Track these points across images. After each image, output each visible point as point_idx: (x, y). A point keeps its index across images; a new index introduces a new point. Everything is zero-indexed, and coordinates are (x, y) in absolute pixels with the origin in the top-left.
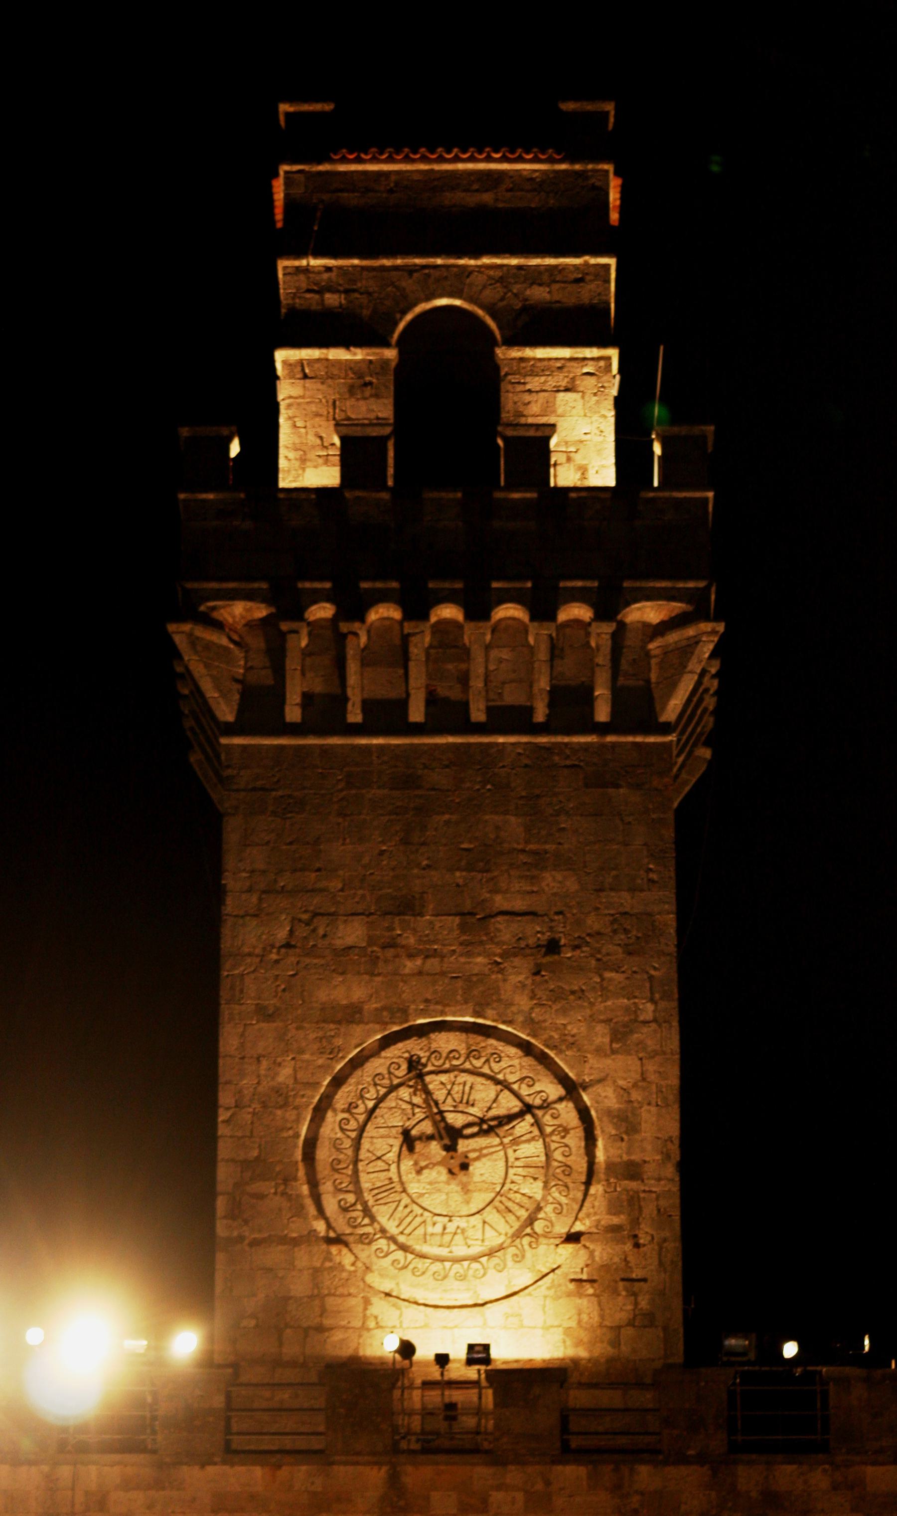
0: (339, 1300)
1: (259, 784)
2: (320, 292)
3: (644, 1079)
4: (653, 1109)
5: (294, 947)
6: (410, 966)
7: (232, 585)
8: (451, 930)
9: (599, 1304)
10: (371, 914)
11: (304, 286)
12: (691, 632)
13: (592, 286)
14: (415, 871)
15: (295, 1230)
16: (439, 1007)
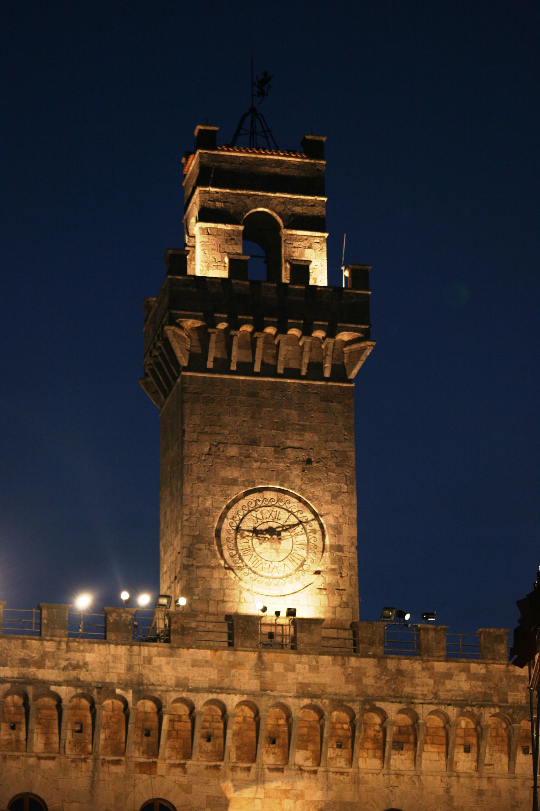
0: (230, 591)
1: (197, 391)
2: (214, 201)
3: (344, 514)
4: (347, 526)
5: (211, 455)
6: (255, 465)
7: (189, 313)
8: (271, 453)
9: (328, 598)
10: (240, 444)
11: (208, 198)
12: (363, 345)
13: (318, 208)
14: (257, 429)
15: (213, 563)
16: (267, 482)
